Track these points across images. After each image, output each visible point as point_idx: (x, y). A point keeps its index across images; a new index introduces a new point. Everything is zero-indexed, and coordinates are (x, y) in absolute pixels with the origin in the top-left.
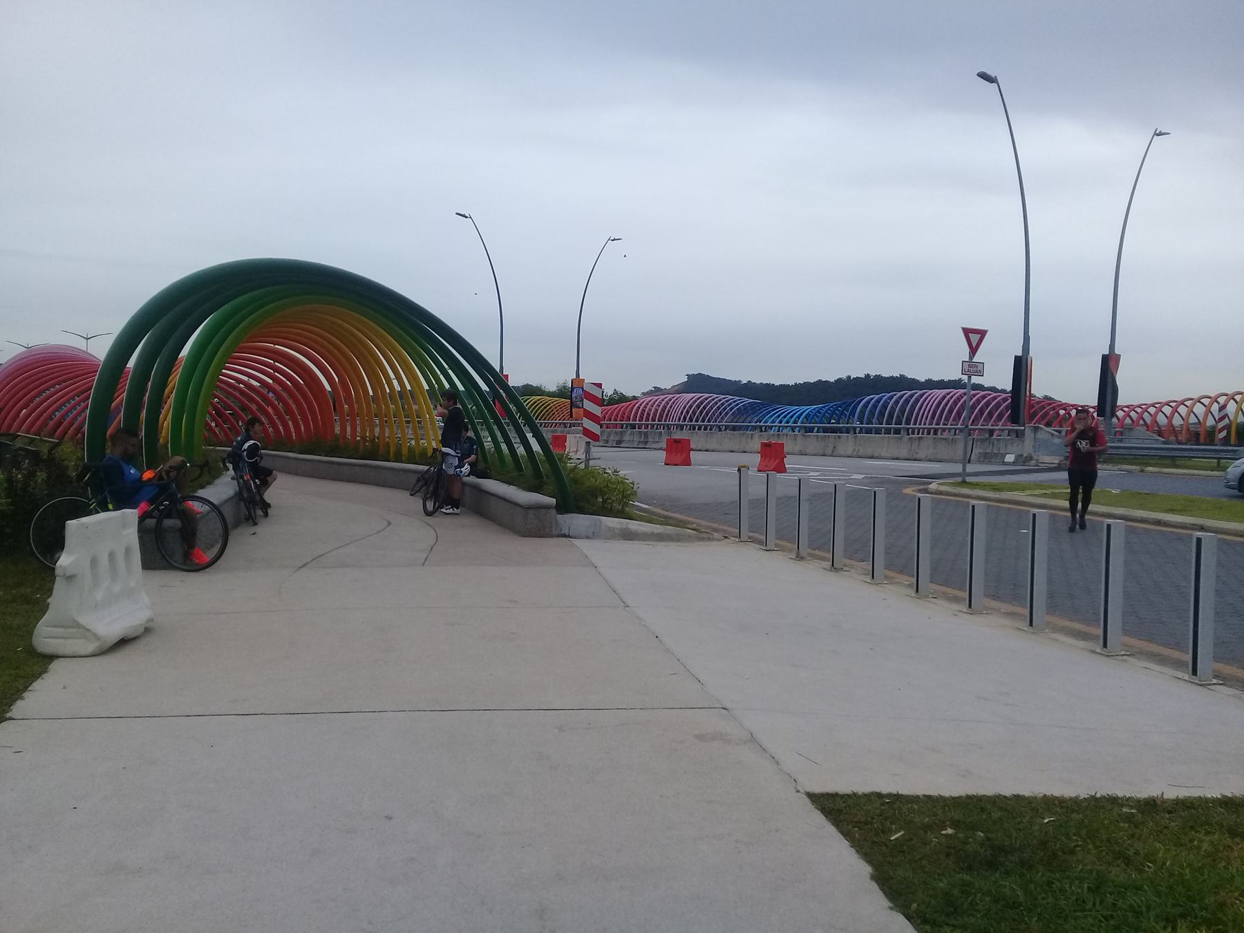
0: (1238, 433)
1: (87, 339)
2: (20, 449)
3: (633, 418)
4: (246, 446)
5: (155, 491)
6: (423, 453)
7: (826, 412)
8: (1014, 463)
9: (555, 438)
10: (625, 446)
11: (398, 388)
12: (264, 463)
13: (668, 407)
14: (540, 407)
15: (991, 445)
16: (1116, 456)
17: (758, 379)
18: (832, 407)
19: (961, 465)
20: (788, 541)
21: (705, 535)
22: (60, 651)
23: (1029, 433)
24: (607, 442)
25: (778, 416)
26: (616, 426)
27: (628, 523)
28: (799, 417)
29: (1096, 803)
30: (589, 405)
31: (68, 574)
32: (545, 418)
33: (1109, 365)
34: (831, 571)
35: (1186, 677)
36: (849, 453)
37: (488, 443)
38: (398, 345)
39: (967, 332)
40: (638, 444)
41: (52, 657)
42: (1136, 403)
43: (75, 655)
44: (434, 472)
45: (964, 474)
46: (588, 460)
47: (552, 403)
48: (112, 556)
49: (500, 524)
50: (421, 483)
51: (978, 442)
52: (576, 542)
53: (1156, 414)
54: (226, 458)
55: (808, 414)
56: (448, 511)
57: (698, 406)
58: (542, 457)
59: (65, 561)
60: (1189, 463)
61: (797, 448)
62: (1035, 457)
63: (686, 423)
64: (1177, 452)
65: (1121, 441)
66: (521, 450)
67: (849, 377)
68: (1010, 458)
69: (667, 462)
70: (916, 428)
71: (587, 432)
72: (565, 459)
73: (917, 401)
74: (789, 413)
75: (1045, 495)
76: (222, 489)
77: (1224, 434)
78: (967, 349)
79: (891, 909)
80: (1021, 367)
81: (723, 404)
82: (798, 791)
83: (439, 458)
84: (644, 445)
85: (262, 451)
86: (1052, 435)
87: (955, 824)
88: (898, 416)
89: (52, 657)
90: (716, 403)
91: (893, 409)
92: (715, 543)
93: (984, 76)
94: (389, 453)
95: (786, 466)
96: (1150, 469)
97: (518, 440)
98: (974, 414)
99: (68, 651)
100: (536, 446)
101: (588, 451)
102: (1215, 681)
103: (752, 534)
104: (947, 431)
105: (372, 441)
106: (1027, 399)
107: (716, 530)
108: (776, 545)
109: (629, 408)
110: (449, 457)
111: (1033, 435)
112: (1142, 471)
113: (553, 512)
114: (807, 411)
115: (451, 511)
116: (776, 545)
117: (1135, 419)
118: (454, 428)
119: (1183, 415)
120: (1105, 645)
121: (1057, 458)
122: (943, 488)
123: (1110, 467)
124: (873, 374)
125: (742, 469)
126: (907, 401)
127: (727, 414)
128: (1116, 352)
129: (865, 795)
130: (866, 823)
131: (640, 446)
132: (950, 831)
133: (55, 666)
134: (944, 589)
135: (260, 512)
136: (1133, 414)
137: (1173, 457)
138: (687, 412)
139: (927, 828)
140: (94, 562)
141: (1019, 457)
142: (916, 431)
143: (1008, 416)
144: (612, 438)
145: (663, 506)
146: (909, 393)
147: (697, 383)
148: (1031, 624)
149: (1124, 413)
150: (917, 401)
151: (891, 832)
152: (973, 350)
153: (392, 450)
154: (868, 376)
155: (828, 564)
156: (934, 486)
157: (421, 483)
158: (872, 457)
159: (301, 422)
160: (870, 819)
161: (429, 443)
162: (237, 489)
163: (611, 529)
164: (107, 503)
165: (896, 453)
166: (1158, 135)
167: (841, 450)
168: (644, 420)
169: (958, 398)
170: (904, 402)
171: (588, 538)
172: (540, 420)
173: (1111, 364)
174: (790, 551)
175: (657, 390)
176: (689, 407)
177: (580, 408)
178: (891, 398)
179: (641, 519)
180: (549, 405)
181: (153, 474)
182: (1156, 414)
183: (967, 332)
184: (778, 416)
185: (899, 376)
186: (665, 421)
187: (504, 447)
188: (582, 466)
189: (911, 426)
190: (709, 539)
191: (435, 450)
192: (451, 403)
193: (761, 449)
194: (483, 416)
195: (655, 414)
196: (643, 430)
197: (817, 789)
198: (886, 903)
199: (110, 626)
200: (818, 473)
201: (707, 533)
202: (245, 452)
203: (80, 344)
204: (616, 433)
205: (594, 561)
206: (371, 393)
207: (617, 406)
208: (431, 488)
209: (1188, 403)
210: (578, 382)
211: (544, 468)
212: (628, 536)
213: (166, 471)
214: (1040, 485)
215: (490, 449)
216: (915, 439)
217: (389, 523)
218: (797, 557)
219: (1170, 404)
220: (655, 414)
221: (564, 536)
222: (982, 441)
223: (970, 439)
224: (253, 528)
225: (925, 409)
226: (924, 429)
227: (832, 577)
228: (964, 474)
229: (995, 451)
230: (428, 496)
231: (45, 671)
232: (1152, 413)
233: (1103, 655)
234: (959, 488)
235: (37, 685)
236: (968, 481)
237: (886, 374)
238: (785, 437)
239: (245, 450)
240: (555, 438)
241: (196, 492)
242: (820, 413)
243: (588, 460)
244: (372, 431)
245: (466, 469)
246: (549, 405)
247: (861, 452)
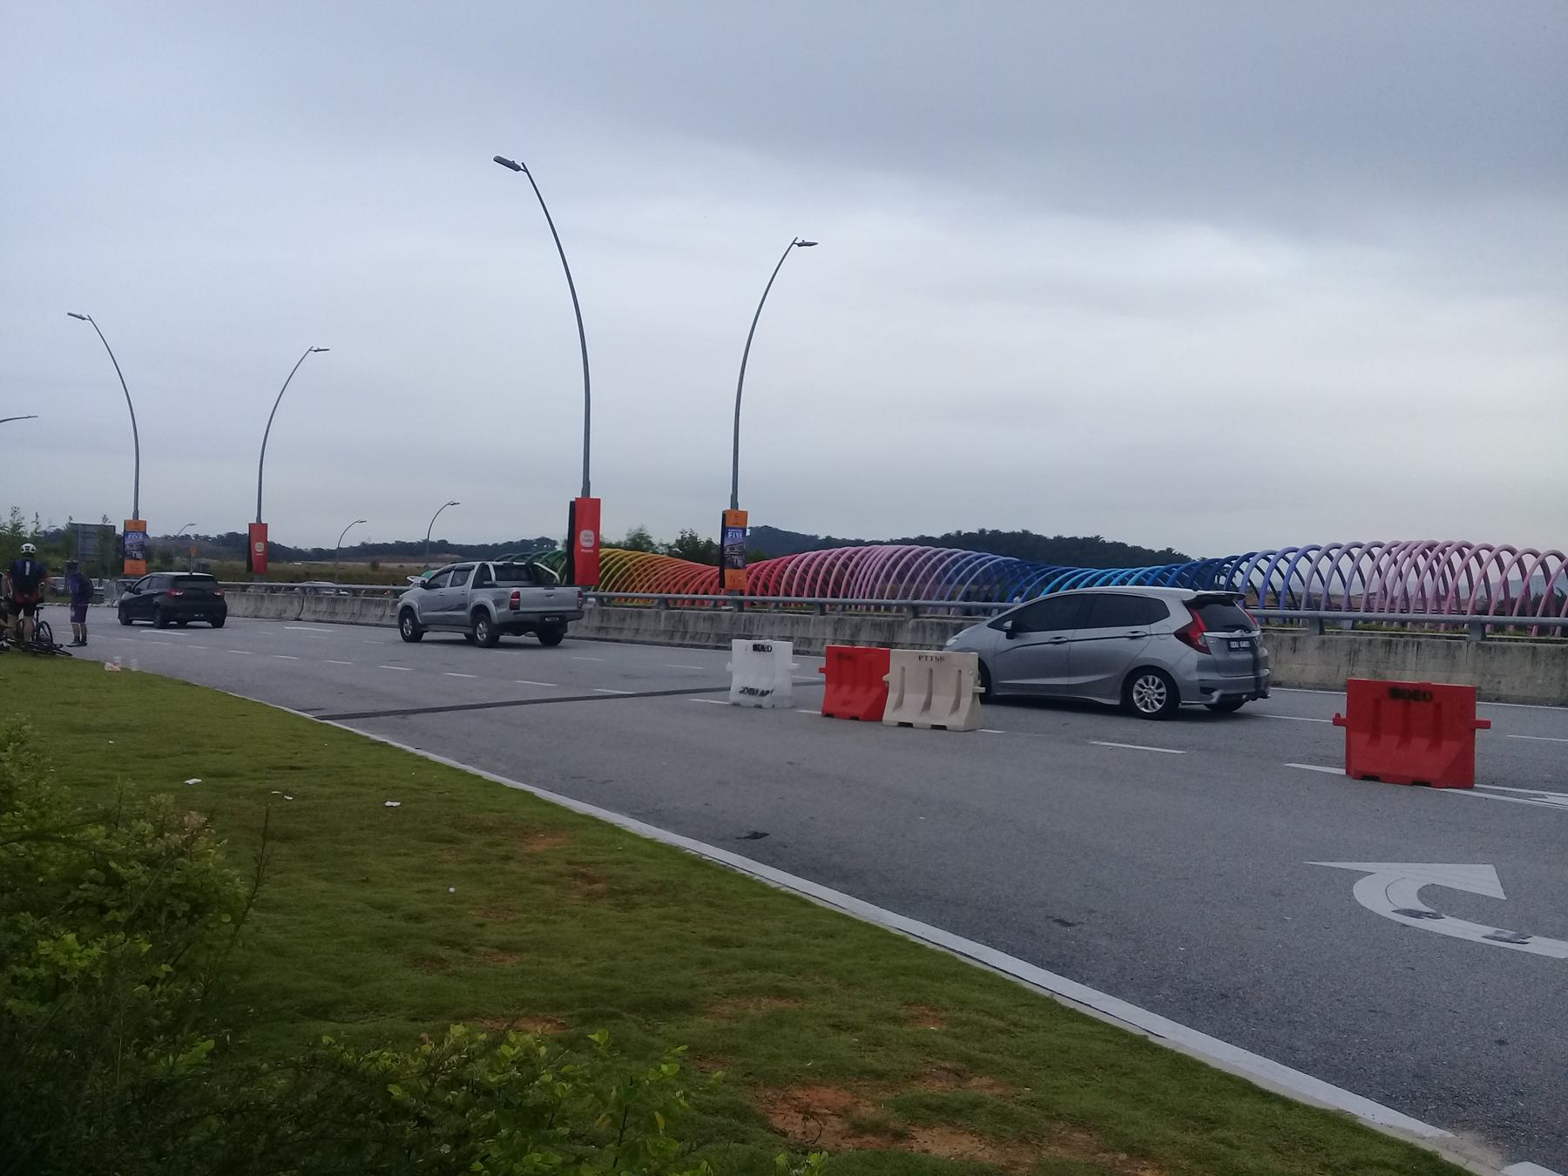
3: (785, 590)
13: (852, 565)
47: (631, 560)
67: (959, 532)
104: (1443, 625)
109: (816, 563)
119: (1305, 576)
124: (989, 528)
128: (263, 522)
154: (982, 531)
177: (739, 568)
180: (625, 564)
185: (1021, 532)
204: (876, 626)
209: (1290, 556)
238: (1412, 650)
246: (625, 564)
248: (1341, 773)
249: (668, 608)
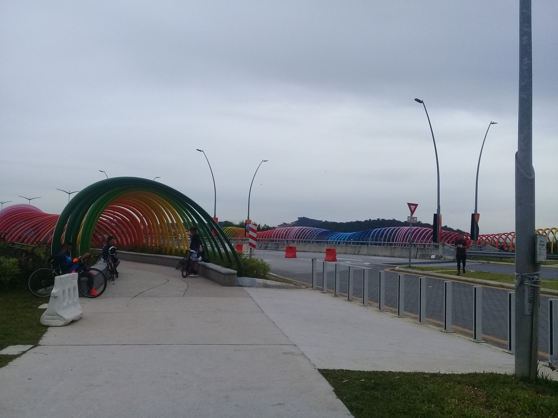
1: (30, 200)
2: (19, 249)
4: (110, 249)
5: (78, 266)
6: (182, 252)
7: (357, 235)
8: (435, 259)
9: (238, 245)
10: (269, 249)
11: (170, 222)
12: (117, 256)
13: (289, 230)
14: (232, 232)
15: (425, 251)
16: (478, 257)
17: (330, 220)
18: (360, 233)
19: (409, 259)
20: (345, 292)
21: (299, 287)
22: (51, 324)
23: (441, 247)
24: (261, 247)
25: (337, 237)
26: (265, 240)
27: (266, 281)
28: (346, 237)
29: (415, 374)
30: (251, 233)
31: (56, 296)
32: (234, 236)
33: (475, 218)
34: (348, 301)
35: (507, 351)
36: (365, 253)
37: (209, 248)
38: (172, 207)
39: (409, 205)
40: (274, 249)
41: (48, 327)
42: (490, 234)
43: (56, 325)
44: (186, 260)
45: (410, 263)
46: (251, 255)
48: (69, 290)
49: (214, 281)
50: (180, 264)
51: (420, 250)
52: (244, 288)
53: (499, 238)
54: (102, 254)
55: (350, 236)
56: (192, 276)
57: (302, 232)
58: (231, 254)
59: (54, 291)
60: (510, 260)
61: (343, 251)
62: (443, 257)
63: (277, 239)
64: (475, 254)
65: (481, 250)
66: (223, 251)
67: (370, 220)
68: (433, 257)
69: (286, 257)
70: (396, 243)
71: (251, 244)
72: (241, 254)
73: (397, 231)
74: (341, 236)
75: (443, 272)
76: (101, 265)
78: (410, 212)
79: (337, 398)
80: (437, 218)
81: (312, 231)
82: (315, 369)
83: (189, 254)
84: (277, 249)
85: (117, 251)
86: (451, 247)
87: (366, 378)
88: (388, 238)
89: (48, 327)
90: (309, 231)
91: (386, 235)
92: (302, 290)
93: (417, 100)
94: (167, 252)
95: (337, 259)
96: (492, 262)
97: (221, 246)
98: (422, 237)
99: (54, 325)
100: (229, 249)
101: (251, 252)
102: (483, 341)
103: (317, 286)
105: (160, 246)
106: (440, 232)
107: (304, 285)
108: (327, 291)
109: (271, 233)
110: (193, 254)
111: (442, 247)
112: (488, 263)
113: (236, 276)
114: (349, 235)
115: (193, 276)
116: (327, 291)
117: (490, 240)
118: (196, 242)
120: (445, 329)
121: (453, 257)
122: (401, 269)
123: (474, 261)
124: (381, 218)
125: (314, 260)
127: (314, 236)
129: (338, 370)
130: (336, 378)
131: (275, 249)
132: (363, 380)
133: (49, 329)
134: (391, 308)
135: (115, 276)
136: (489, 238)
137: (501, 257)
138: (297, 235)
139: (356, 379)
140: (64, 292)
141: (437, 256)
142: (396, 245)
143: (432, 237)
144: (263, 246)
145: (282, 275)
147: (303, 221)
148: (420, 321)
149: (505, 236)
150: (397, 231)
151: (343, 380)
152: (412, 212)
153: (168, 250)
154: (379, 219)
155: (347, 298)
156: (397, 268)
157: (180, 264)
158: (375, 255)
159: (128, 238)
160: (337, 377)
161: (184, 247)
162: (107, 266)
163: (259, 283)
164: (60, 271)
165: (385, 254)
166: (492, 124)
167: (361, 252)
168: (275, 237)
169: (414, 230)
170: (391, 232)
171: (250, 287)
172: (231, 237)
173: (476, 217)
174: (332, 293)
175: (285, 225)
178: (385, 230)
179: (273, 280)
180: (236, 231)
181: (78, 260)
182: (499, 238)
183: (409, 205)
184: (337, 237)
185: (392, 219)
186: (287, 238)
187: (216, 249)
188: (248, 258)
189: (394, 242)
190: (300, 288)
191: (187, 251)
192: (194, 232)
193: (326, 251)
194: (207, 236)
195: (282, 235)
196: (277, 242)
197: (322, 368)
198: (336, 396)
199: (69, 315)
200: (350, 262)
201: (299, 286)
202: (110, 251)
203: (26, 202)
204: (265, 243)
205: (251, 295)
206: (159, 224)
207: (266, 231)
208: (186, 266)
210: (248, 221)
211: (233, 259)
212: (266, 286)
213: (83, 259)
214: (441, 268)
215: (210, 250)
216: (393, 248)
217: (168, 281)
218: (335, 295)
219: (505, 234)
220: (282, 235)
221: (240, 286)
222: (421, 249)
223: (416, 248)
224: (113, 282)
225: (400, 235)
226: (400, 244)
227: (348, 303)
228: (410, 263)
229: (427, 254)
230: (184, 269)
231: (47, 331)
232: (504, 238)
233: (508, 353)
234: (407, 269)
235: (45, 335)
236: (411, 266)
237: (386, 219)
239: (110, 250)
240: (238, 245)
241: (91, 267)
242: (355, 236)
243: (251, 255)
244: (160, 242)
245: (200, 258)
246: (236, 231)
247: (370, 254)
248: (455, 265)
249: (271, 242)
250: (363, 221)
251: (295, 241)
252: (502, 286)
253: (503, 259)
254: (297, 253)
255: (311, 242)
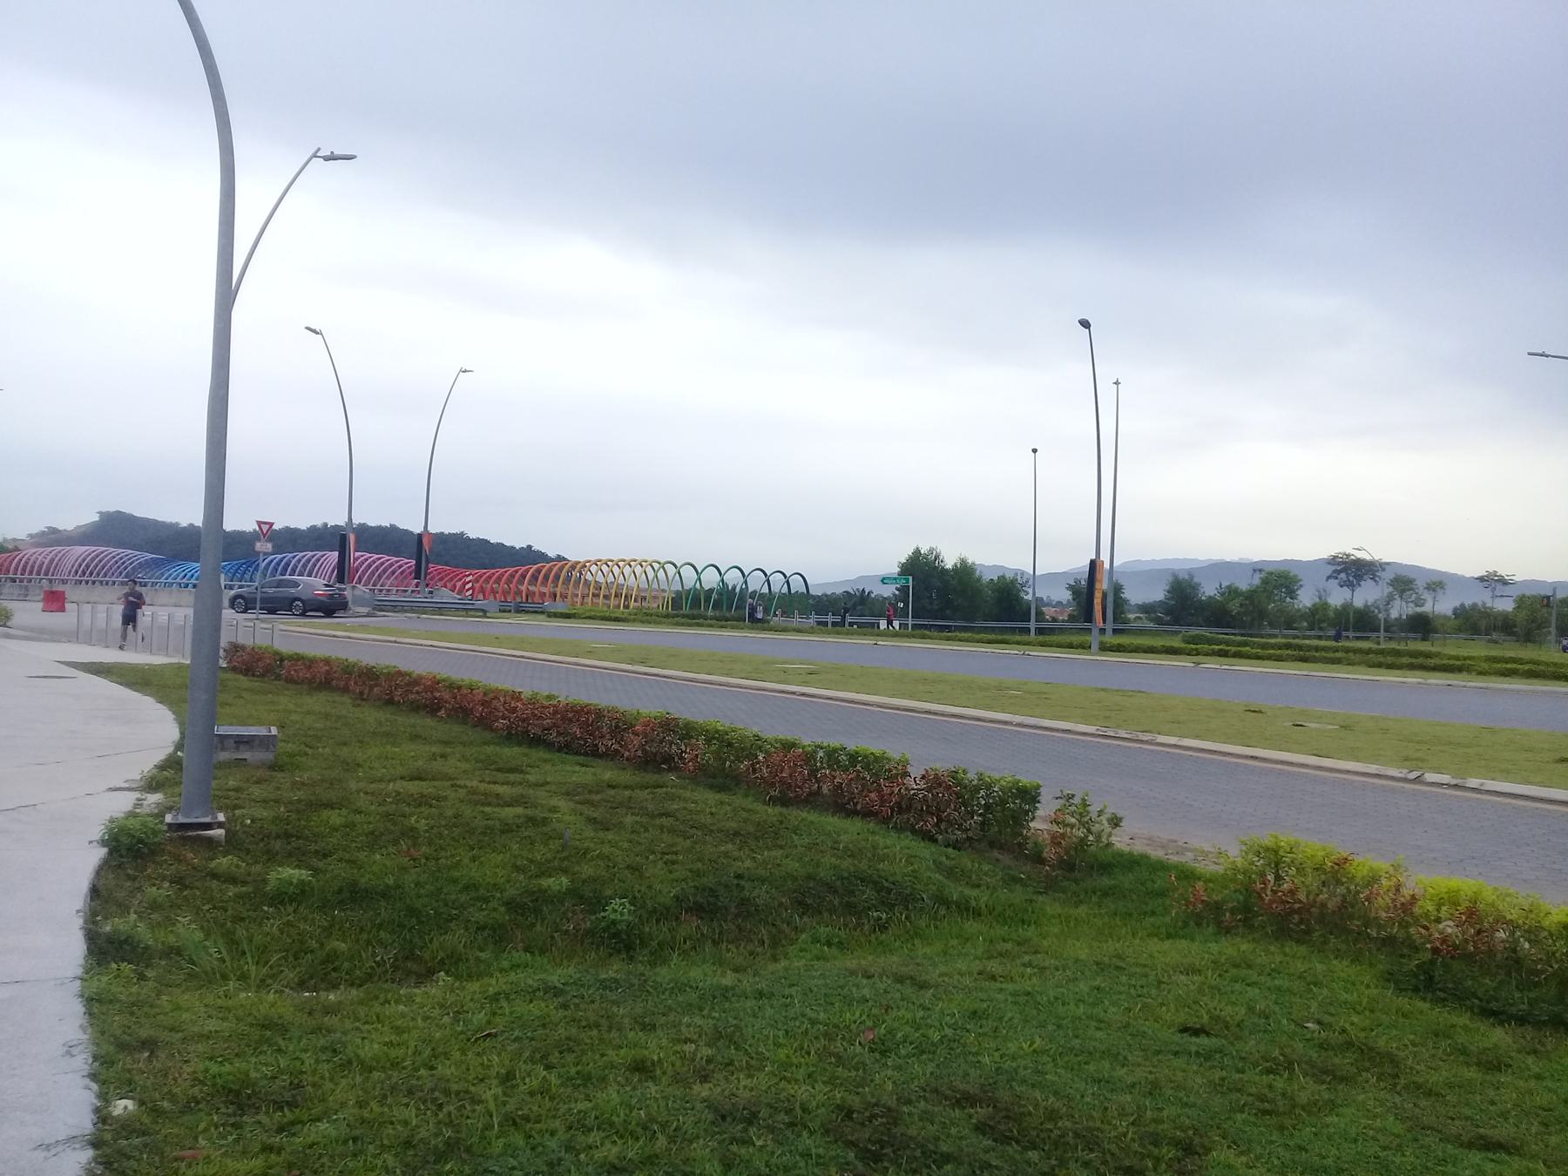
0: (1560, 616)
63: (26, 576)
67: (326, 525)
73: (318, 560)
77: (470, 592)
81: (121, 559)
126: (309, 561)
138: (80, 565)
146: (280, 556)
150: (318, 560)
176: (303, 566)
250: (303, 527)
251: (67, 580)
252: (350, 638)
253: (470, 613)
254: (67, 605)
255: (110, 583)
